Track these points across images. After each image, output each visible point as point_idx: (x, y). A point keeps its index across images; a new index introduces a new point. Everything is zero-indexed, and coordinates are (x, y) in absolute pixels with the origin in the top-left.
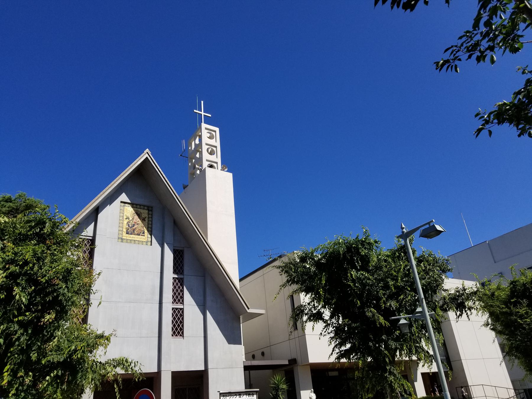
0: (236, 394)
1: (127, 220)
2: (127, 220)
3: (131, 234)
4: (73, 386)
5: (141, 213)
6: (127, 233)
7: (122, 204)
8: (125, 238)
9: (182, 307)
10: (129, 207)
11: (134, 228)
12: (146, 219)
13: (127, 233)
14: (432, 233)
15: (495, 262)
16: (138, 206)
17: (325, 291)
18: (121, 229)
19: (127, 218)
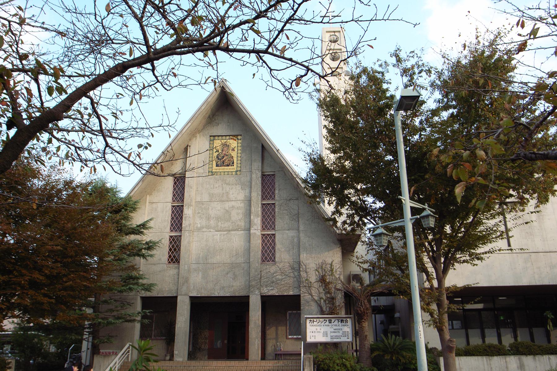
0: (326, 319)
1: (217, 153)
2: (217, 153)
3: (221, 166)
4: (78, 304)
5: (230, 143)
6: (217, 166)
7: (212, 138)
8: (215, 171)
9: (273, 233)
10: (473, 284)
11: (224, 159)
12: (236, 149)
13: (217, 166)
14: (517, 251)
15: (276, 355)
16: (224, 137)
17: (466, 216)
18: (234, 173)
19: (218, 151)
